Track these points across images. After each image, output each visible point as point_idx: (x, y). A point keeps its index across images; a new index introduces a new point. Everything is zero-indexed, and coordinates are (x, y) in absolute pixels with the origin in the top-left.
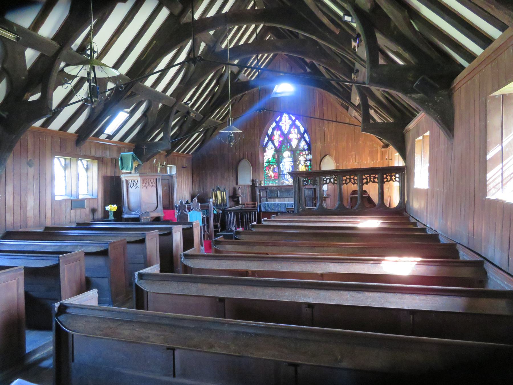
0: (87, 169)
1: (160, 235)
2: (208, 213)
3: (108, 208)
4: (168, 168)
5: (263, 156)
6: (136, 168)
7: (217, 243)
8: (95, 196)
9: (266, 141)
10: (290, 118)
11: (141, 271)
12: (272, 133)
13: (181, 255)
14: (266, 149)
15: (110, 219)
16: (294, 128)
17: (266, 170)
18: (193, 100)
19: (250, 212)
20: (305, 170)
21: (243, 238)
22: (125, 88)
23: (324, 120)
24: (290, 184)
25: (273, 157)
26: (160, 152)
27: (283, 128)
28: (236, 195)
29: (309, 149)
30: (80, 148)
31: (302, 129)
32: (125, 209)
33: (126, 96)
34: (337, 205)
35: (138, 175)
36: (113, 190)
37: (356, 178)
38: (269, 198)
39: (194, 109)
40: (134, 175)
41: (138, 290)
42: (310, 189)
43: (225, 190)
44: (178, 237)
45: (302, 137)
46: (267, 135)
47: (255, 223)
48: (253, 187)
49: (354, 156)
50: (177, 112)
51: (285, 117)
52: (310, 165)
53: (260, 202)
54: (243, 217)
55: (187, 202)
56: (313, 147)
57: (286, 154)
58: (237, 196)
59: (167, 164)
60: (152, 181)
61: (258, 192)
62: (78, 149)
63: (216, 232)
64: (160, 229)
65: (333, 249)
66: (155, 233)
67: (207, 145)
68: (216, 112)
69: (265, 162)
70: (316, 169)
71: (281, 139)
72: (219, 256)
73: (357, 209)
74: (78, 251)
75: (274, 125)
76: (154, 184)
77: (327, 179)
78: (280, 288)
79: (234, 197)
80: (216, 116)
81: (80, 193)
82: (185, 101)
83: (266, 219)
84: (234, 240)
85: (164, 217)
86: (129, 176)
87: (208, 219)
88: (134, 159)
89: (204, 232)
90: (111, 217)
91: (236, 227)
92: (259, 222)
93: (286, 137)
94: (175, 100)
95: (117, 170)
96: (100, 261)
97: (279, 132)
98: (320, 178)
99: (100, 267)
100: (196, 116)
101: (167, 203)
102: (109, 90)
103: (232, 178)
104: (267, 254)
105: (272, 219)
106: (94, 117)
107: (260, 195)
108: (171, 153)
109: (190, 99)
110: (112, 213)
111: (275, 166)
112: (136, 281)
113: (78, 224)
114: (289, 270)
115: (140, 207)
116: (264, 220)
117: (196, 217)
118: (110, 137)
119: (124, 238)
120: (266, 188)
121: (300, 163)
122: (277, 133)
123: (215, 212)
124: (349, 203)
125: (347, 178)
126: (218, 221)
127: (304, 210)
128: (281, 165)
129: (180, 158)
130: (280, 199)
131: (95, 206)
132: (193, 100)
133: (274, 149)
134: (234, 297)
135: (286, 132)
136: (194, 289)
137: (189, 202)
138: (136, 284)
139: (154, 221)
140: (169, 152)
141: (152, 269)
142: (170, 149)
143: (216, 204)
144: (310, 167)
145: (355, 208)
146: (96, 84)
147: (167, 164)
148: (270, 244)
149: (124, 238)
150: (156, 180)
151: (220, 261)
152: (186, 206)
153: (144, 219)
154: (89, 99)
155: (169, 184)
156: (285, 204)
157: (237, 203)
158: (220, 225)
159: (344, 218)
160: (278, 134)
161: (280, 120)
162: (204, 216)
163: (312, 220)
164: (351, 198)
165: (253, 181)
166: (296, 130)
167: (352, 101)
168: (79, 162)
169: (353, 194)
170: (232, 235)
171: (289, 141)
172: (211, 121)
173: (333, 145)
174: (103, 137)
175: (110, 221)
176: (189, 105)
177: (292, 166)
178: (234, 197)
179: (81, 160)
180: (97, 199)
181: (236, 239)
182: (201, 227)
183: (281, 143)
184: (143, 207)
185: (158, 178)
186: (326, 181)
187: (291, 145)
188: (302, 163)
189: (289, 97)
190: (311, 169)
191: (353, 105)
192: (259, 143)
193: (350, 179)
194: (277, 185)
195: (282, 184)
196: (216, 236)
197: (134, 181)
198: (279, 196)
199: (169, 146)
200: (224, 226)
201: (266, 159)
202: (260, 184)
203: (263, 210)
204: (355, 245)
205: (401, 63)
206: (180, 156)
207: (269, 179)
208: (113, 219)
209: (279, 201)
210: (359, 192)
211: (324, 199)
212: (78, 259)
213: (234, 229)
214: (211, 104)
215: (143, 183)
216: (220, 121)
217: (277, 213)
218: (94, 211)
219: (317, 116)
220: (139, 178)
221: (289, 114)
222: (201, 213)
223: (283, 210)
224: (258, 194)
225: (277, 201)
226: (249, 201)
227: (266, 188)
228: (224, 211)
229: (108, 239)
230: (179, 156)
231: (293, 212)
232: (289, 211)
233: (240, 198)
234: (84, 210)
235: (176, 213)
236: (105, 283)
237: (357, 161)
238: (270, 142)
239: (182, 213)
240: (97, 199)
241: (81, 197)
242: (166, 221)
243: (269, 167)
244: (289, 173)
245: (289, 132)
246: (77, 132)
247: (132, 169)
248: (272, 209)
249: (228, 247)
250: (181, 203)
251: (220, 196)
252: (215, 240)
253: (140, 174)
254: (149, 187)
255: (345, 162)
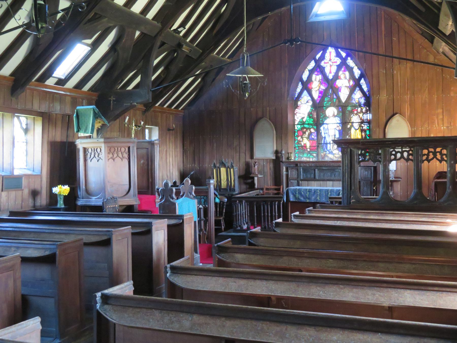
0: (26, 131)
1: (133, 234)
2: (207, 201)
3: (56, 190)
4: (147, 131)
5: (294, 114)
6: (98, 130)
7: (222, 250)
8: (37, 172)
9: (299, 90)
10: (338, 55)
11: (106, 291)
12: (310, 77)
13: (166, 267)
14: (299, 103)
15: (58, 206)
16: (344, 71)
17: (298, 136)
18: (187, 26)
19: (271, 202)
20: (360, 137)
21: (262, 242)
22: (87, 6)
23: (393, 57)
24: (335, 159)
25: (310, 115)
26: (135, 106)
27: (327, 71)
28: (250, 174)
29: (368, 104)
30: (17, 98)
31: (357, 73)
32: (81, 192)
33: (86, 20)
34: (412, 195)
35: (102, 140)
36: (64, 162)
37: (445, 152)
38: (302, 180)
39: (188, 40)
40: (96, 140)
41: (102, 321)
42: (367, 168)
43: (232, 167)
44: (160, 237)
45: (357, 84)
46: (301, 80)
47: (280, 220)
48: (277, 162)
49: (441, 117)
50: (163, 44)
51: (331, 51)
52: (369, 130)
53: (287, 186)
54: (261, 209)
55: (175, 184)
56: (373, 100)
57: (331, 111)
58: (252, 175)
59: (145, 124)
60: (123, 149)
61: (284, 169)
62: (14, 99)
63: (218, 231)
64: (133, 225)
65: (407, 266)
66: (126, 231)
67: (205, 97)
68: (222, 45)
69: (296, 123)
70: (378, 136)
71: (323, 87)
72: (223, 270)
73: (445, 202)
74: (10, 256)
75: (312, 64)
76: (126, 155)
77: (397, 152)
78: (324, 329)
79: (247, 177)
80: (221, 52)
81: (15, 166)
82: (175, 27)
83: (297, 213)
84: (246, 246)
85: (139, 205)
86: (87, 142)
87: (206, 211)
88: (96, 116)
89: (200, 230)
90: (61, 204)
91: (249, 224)
92: (286, 218)
93: (330, 85)
94: (159, 25)
95: (70, 133)
96: (43, 272)
97: (320, 77)
98: (385, 152)
99: (43, 280)
100: (190, 51)
101: (145, 184)
102: (63, 10)
103: (244, 147)
104: (300, 271)
105: (307, 214)
106: (41, 49)
107: (287, 175)
108: (151, 107)
109: (183, 24)
110: (62, 197)
111: (312, 130)
112: (98, 306)
113: (12, 213)
114: (337, 298)
115: (103, 189)
116: (294, 216)
117: (188, 208)
118: (61, 82)
119: (80, 237)
120: (297, 165)
121: (352, 126)
122: (317, 78)
123: (217, 200)
124: (433, 192)
125: (429, 152)
126: (221, 214)
127: (358, 201)
128: (322, 128)
129: (165, 115)
130: (319, 182)
131: (37, 187)
132: (187, 26)
133: (311, 103)
134: (250, 339)
135: (330, 77)
136: (186, 323)
137: (178, 183)
138: (98, 311)
139: (123, 211)
140: (148, 106)
141: (122, 288)
142: (151, 101)
143: (218, 188)
144: (368, 132)
145: (442, 200)
146: (44, 2)
147: (145, 124)
148: (306, 255)
149: (80, 237)
150: (129, 148)
151: (226, 279)
152: (174, 190)
153: (109, 209)
154: (34, 24)
155: (148, 155)
156: (328, 190)
157: (251, 187)
158: (224, 219)
159: (425, 216)
160: (318, 79)
161: (323, 58)
162: (201, 206)
163: (372, 217)
164: (436, 184)
165: (277, 152)
166: (347, 73)
167: (440, 27)
168: (16, 119)
169: (438, 178)
170: (244, 236)
171: (336, 90)
172: (214, 57)
173: (407, 97)
174: (51, 82)
175: (59, 209)
176: (181, 34)
177: (339, 131)
178: (247, 177)
179: (18, 117)
180: (41, 176)
181: (250, 244)
182: (195, 222)
183: (323, 94)
184: (109, 189)
185: (131, 145)
186: (395, 155)
187: (338, 98)
188: (356, 125)
189: (337, 22)
190: (369, 136)
191: (442, 35)
192: (288, 94)
193: (435, 154)
194: (315, 159)
195: (323, 158)
196: (220, 238)
197: (95, 150)
198: (317, 178)
199: (149, 97)
200: (230, 225)
201: (298, 118)
202: (288, 158)
203: (292, 198)
204: (444, 262)
205: (200, 80)
206: (165, 112)
207: (302, 150)
208: (63, 206)
209: (317, 186)
210: (449, 175)
211: (389, 184)
212: (11, 268)
213: (245, 227)
214: (215, 32)
215: (109, 153)
216: (228, 58)
217: (314, 204)
218: (35, 194)
219: (382, 50)
220: (103, 145)
221: (336, 48)
222: (196, 201)
223: (324, 200)
224: (285, 173)
225: (314, 186)
226: (269, 183)
227: (296, 164)
228: (230, 198)
229: (56, 237)
230: (163, 112)
231: (340, 203)
232: (333, 203)
233: (256, 178)
234: (20, 192)
235: (158, 200)
236: (50, 304)
237: (446, 124)
238: (305, 92)
239: (167, 200)
240: (41, 176)
241: (16, 173)
242: (143, 213)
243: (302, 132)
244: (335, 142)
245: (336, 77)
246: (13, 74)
247: (92, 132)
248: (306, 197)
249: (240, 257)
250: (166, 184)
251: (225, 176)
252: (218, 246)
253: (105, 138)
254: (118, 160)
255: (426, 125)
